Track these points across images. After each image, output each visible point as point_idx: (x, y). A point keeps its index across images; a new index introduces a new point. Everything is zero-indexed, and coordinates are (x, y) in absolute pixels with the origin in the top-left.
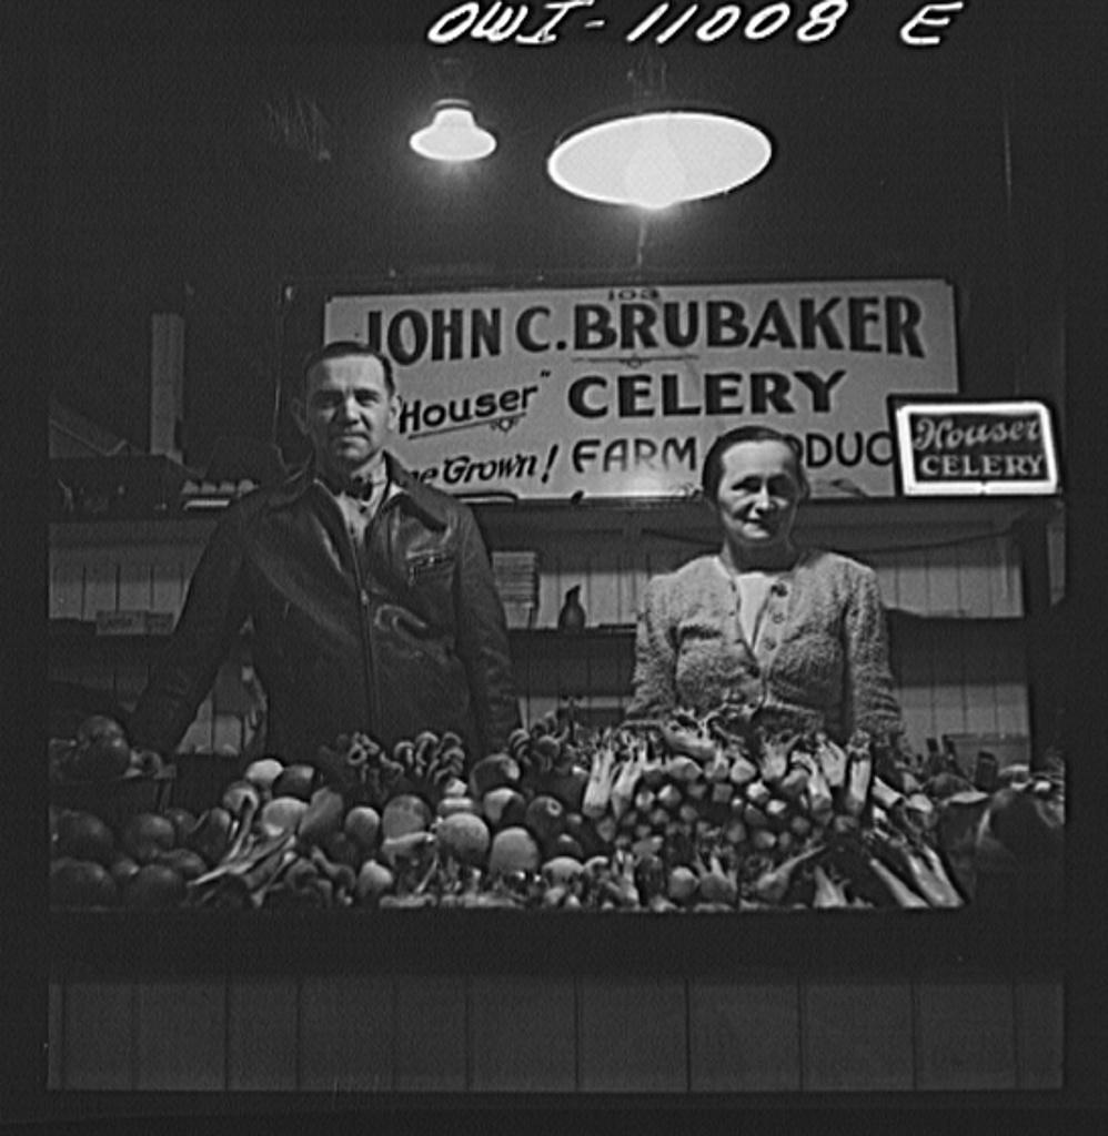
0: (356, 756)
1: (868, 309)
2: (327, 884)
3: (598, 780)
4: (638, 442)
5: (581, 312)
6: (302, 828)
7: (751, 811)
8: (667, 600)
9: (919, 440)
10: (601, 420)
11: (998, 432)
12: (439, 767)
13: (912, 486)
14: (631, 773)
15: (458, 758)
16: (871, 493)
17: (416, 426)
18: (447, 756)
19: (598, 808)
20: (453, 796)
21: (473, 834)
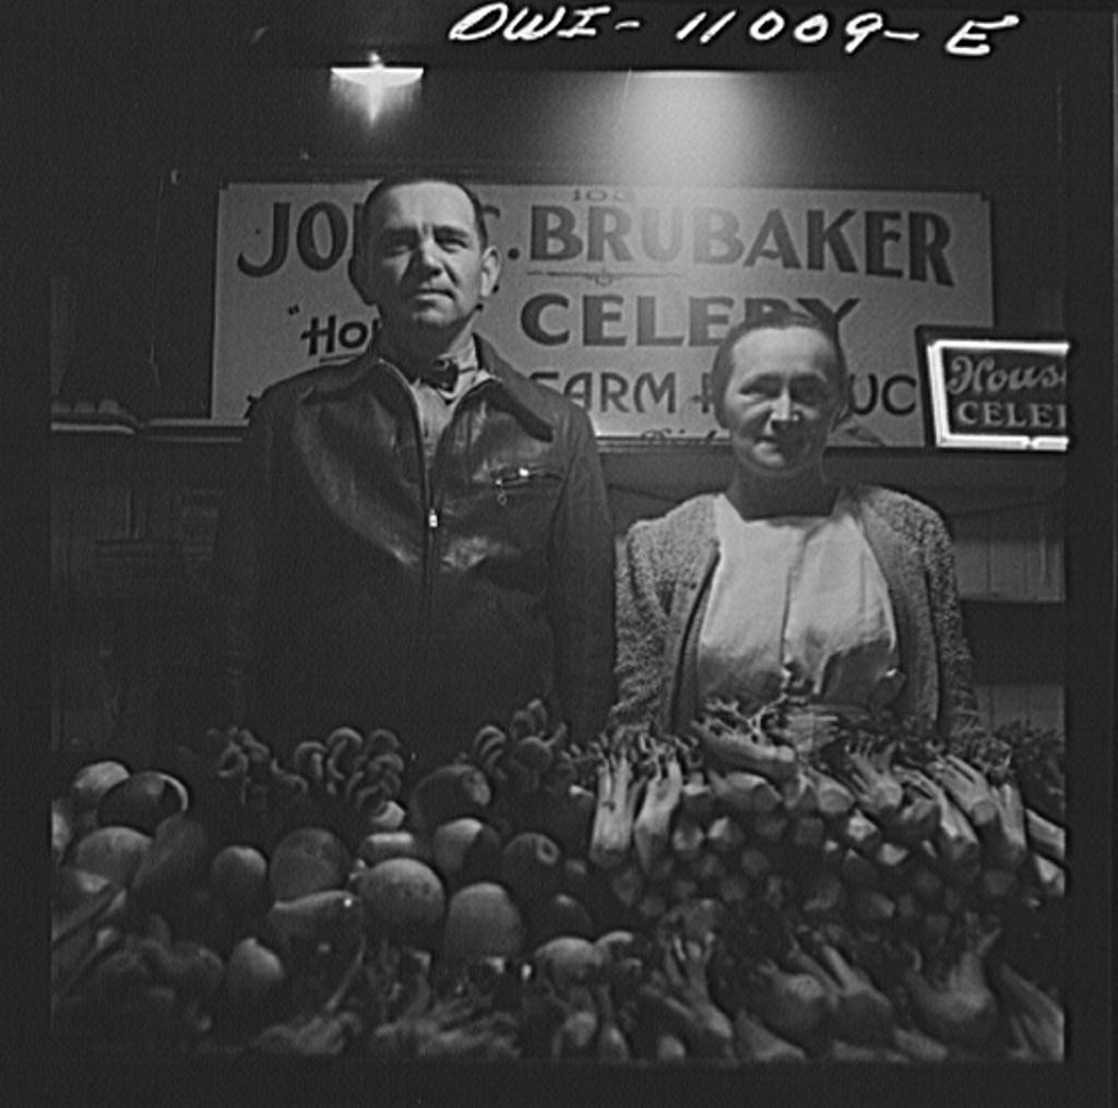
0: (231, 762)
1: (888, 226)
2: (167, 994)
3: (612, 807)
4: (605, 377)
5: (538, 214)
6: (137, 883)
7: (853, 860)
8: (657, 557)
9: (954, 382)
10: (563, 347)
11: (1048, 375)
12: (363, 783)
13: (945, 436)
14: (661, 797)
15: (395, 770)
16: (888, 443)
17: (330, 348)
18: (375, 766)
19: (614, 852)
20: (382, 829)
21: (419, 894)
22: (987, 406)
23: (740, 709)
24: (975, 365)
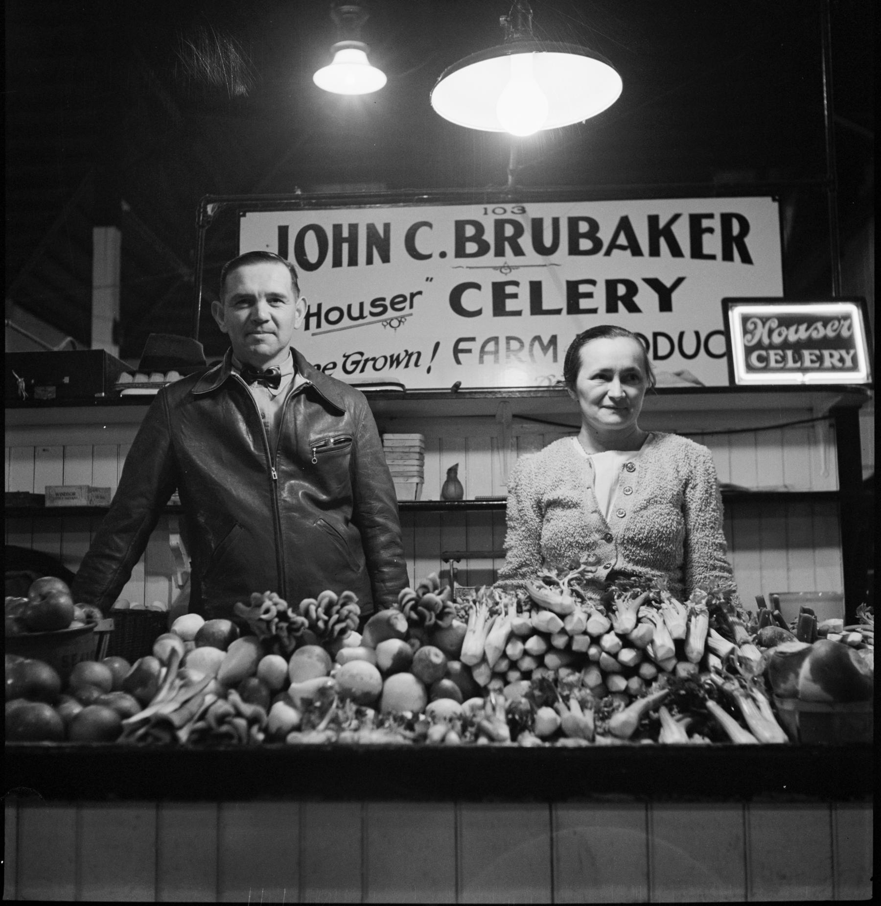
5: (460, 226)
11: (816, 329)
12: (339, 621)
17: (319, 325)
22: (772, 353)
23: (558, 575)
24: (764, 324)
